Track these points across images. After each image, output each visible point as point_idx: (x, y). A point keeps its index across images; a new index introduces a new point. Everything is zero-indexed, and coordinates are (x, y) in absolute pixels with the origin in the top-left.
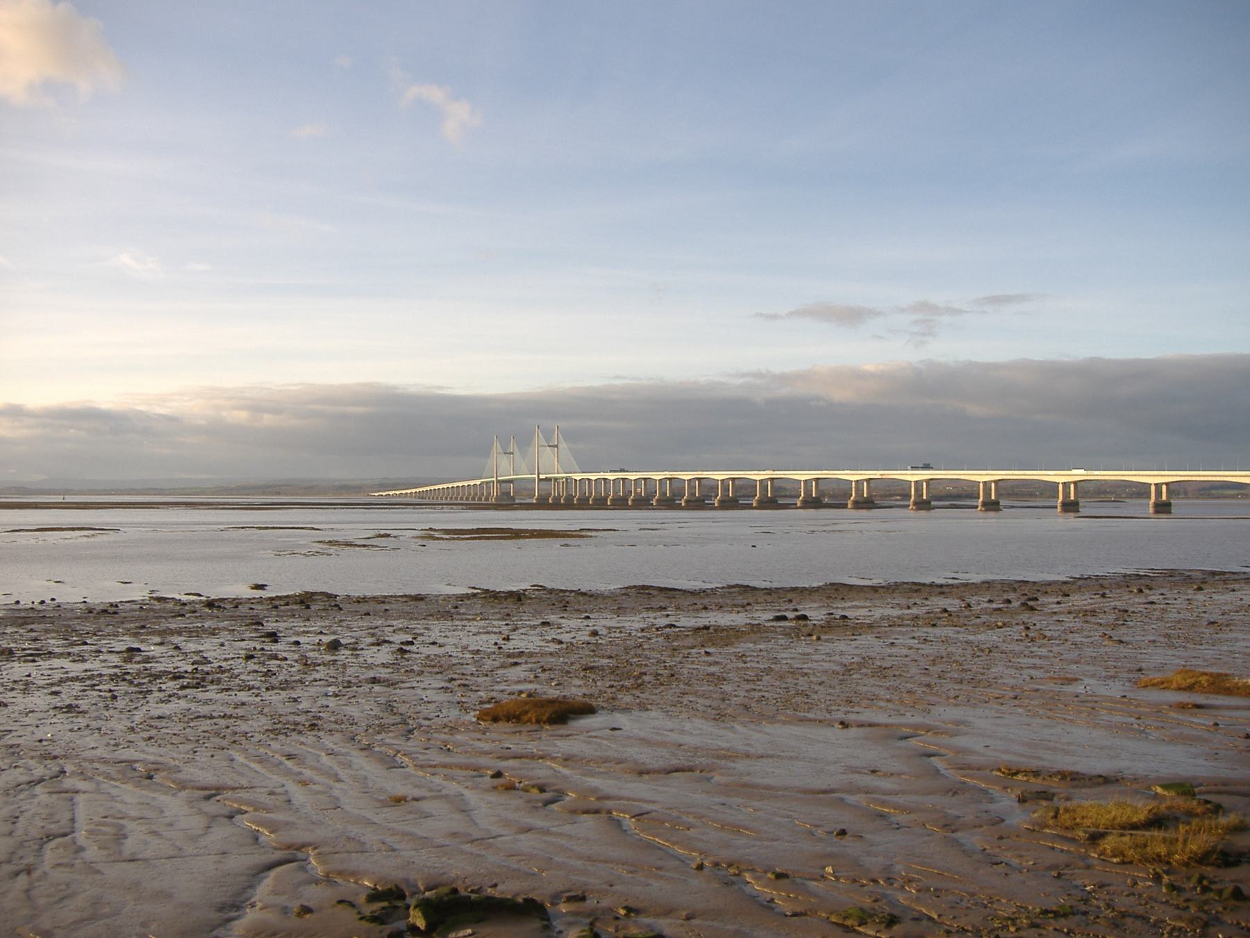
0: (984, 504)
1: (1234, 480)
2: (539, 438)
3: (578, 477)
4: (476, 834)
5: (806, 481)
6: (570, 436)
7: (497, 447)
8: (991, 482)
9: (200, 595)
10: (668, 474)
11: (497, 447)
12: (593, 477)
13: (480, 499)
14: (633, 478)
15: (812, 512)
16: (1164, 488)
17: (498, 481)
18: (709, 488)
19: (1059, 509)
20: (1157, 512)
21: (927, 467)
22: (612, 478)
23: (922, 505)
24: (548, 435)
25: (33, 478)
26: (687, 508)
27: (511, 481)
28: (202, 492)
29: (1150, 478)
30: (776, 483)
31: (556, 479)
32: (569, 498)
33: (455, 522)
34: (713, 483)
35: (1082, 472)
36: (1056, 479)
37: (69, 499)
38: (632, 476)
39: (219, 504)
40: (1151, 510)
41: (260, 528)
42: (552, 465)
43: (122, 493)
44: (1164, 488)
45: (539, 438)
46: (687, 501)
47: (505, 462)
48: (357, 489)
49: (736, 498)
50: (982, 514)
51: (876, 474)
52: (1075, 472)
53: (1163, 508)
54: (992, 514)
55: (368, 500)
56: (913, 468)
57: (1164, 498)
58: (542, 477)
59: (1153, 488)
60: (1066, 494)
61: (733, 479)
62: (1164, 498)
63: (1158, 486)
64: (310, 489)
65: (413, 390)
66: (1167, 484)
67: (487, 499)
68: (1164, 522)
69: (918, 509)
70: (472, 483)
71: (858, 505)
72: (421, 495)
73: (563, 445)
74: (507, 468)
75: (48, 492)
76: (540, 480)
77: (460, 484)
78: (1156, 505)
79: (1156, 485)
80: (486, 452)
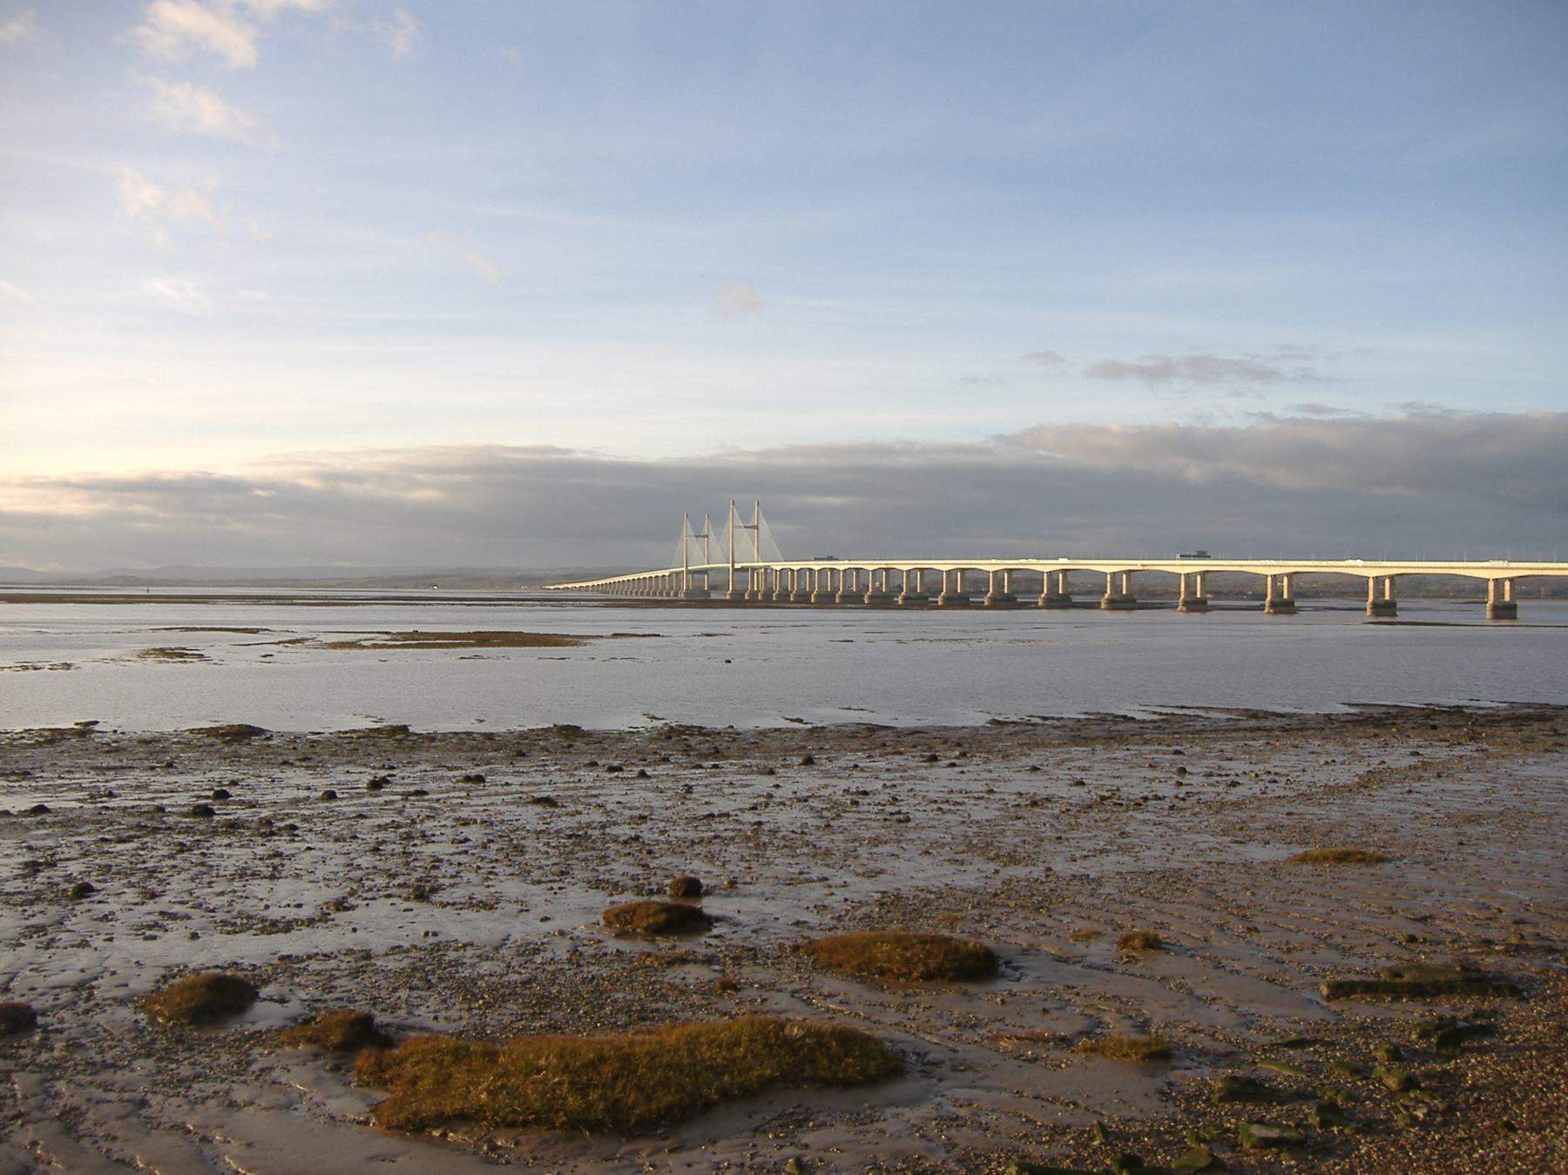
0: (1273, 605)
1: (1351, 571)
2: (733, 518)
3: (777, 566)
4: (1222, 1047)
5: (1274, 577)
6: (770, 516)
7: (687, 529)
8: (1283, 575)
9: (800, 721)
10: (883, 564)
11: (687, 529)
12: (796, 566)
13: (676, 594)
14: (871, 568)
15: (1121, 615)
16: (1387, 582)
17: (689, 572)
18: (976, 582)
19: (1369, 612)
20: (1496, 617)
21: (1202, 555)
22: (816, 568)
23: (1196, 605)
24: (745, 515)
25: (138, 565)
26: (904, 607)
27: (705, 571)
28: (347, 584)
29: (1267, 568)
30: (1015, 575)
31: (753, 569)
32: (768, 593)
33: (505, 622)
34: (980, 576)
35: (1065, 561)
36: (1365, 572)
37: (155, 591)
38: (841, 566)
39: (294, 598)
40: (1489, 614)
41: (187, 629)
42: (748, 550)
43: (253, 584)
44: (1507, 585)
45: (733, 518)
46: (905, 598)
47: (696, 548)
48: (540, 580)
49: (1014, 595)
50: (1269, 618)
51: (1136, 565)
52: (1351, 562)
53: (1504, 611)
54: (1283, 618)
55: (544, 595)
56: (1184, 557)
57: (1507, 598)
58: (737, 566)
59: (1491, 585)
60: (1379, 592)
61: (963, 570)
62: (1507, 598)
63: (1379, 580)
64: (478, 580)
65: (908, 449)
66: (1511, 580)
67: (676, 594)
68: (1505, 630)
69: (1189, 611)
70: (660, 574)
71: (1114, 605)
72: (604, 589)
73: (764, 526)
74: (702, 555)
75: (166, 583)
76: (735, 570)
77: (653, 574)
78: (1495, 608)
79: (1496, 580)
80: (673, 535)
